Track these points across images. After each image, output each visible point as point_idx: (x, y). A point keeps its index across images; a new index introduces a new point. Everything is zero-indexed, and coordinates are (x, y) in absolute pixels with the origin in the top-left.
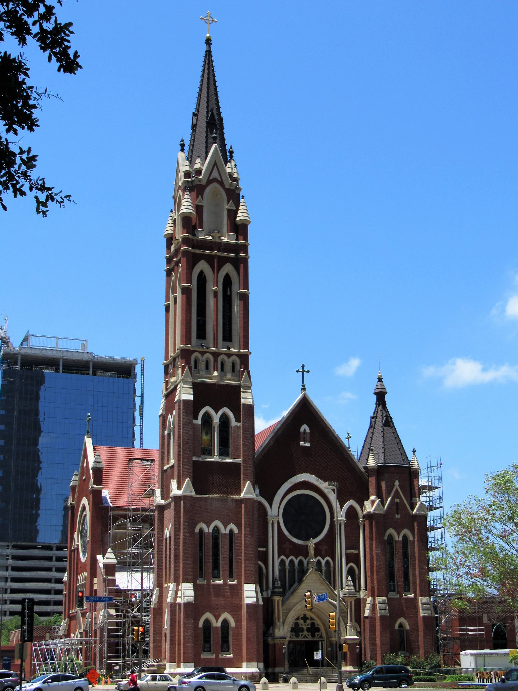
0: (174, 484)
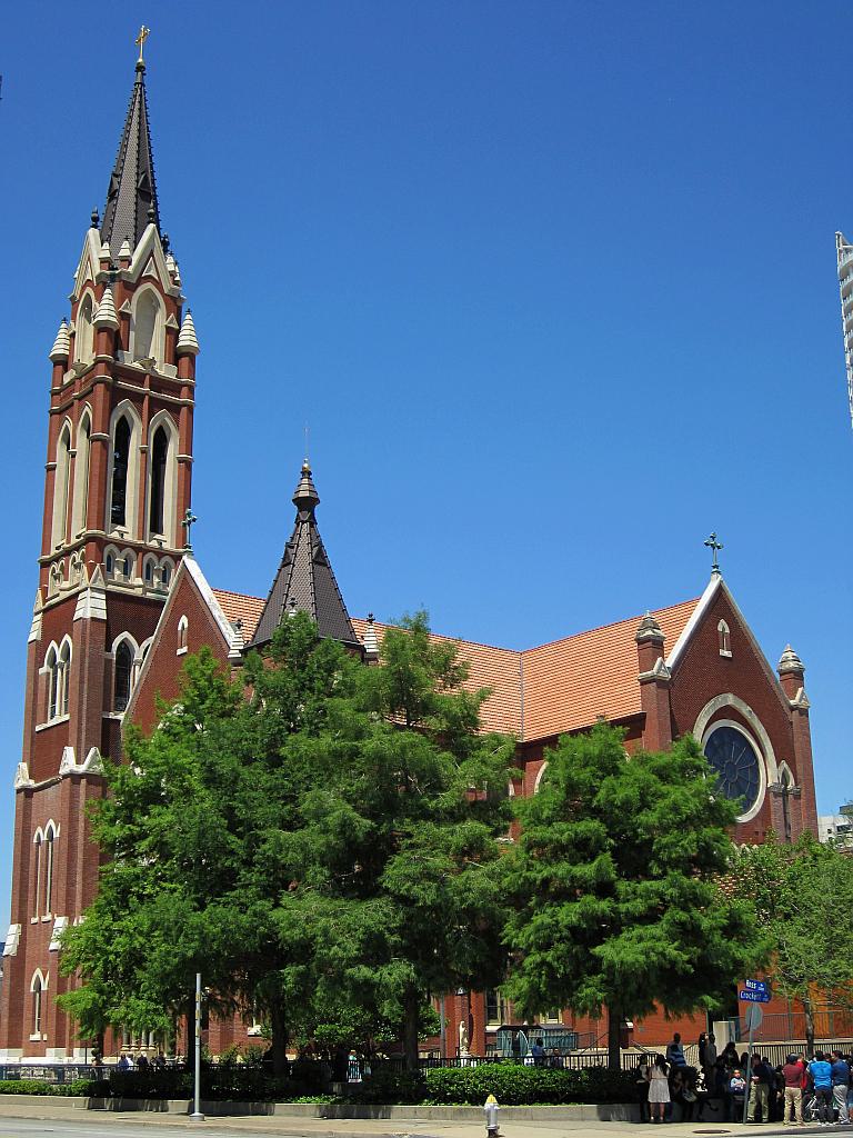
0: (70, 752)
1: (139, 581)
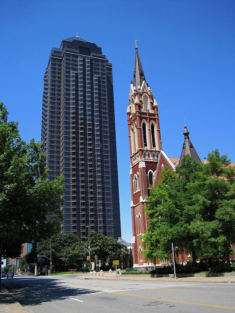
1: (152, 158)
